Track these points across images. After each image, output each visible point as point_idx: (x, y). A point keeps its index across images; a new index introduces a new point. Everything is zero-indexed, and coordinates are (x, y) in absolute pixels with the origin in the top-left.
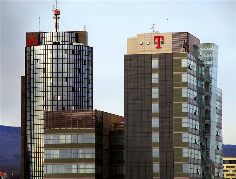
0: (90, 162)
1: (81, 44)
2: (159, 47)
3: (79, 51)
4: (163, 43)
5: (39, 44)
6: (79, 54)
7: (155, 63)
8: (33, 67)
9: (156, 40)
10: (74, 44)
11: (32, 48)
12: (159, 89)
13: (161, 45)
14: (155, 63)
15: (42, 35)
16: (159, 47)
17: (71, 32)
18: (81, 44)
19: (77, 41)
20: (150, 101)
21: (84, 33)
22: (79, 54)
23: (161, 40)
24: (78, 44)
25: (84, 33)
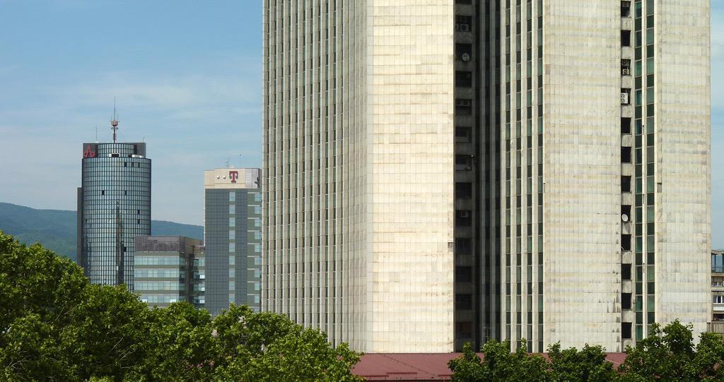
0: (174, 250)
1: (141, 157)
2: (234, 181)
3: (139, 164)
4: (237, 178)
5: (97, 156)
6: (139, 167)
7: (232, 197)
8: (88, 198)
9: (232, 175)
10: (133, 156)
11: (89, 160)
12: (236, 270)
13: (236, 180)
14: (232, 197)
15: (100, 147)
16: (234, 181)
17: (130, 144)
18: (141, 157)
19: (135, 153)
20: (228, 267)
21: (143, 145)
22: (139, 167)
23: (236, 175)
24: (137, 156)
25: (143, 145)
